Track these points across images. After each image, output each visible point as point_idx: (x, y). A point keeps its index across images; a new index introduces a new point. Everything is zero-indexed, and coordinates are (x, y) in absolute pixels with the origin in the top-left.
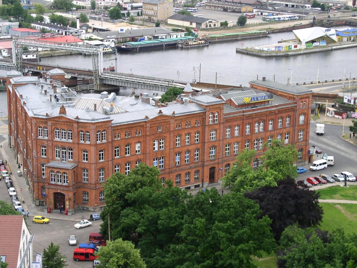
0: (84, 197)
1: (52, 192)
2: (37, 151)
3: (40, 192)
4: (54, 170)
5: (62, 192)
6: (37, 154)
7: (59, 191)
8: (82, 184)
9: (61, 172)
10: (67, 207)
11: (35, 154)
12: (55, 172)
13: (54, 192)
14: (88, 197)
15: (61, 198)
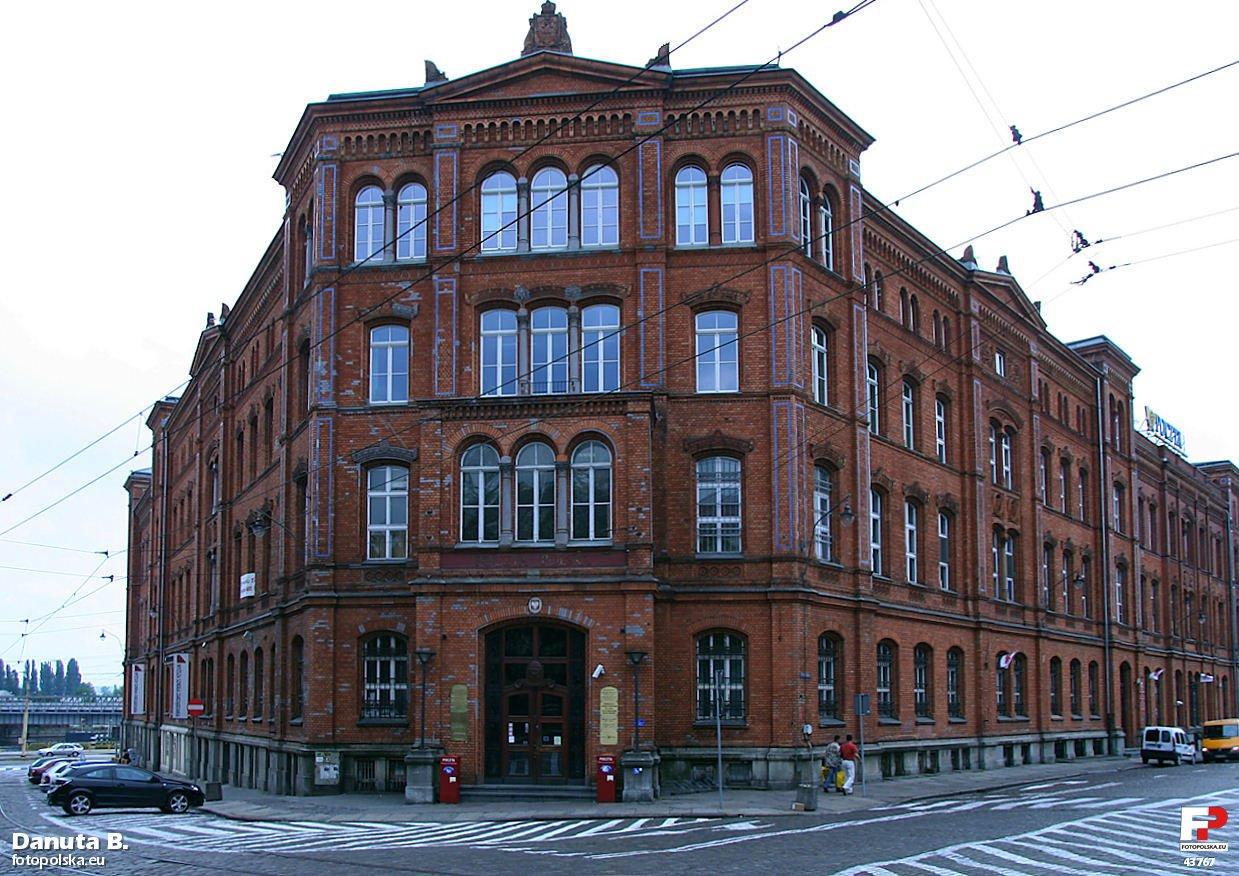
0: (706, 679)
1: (470, 621)
2: (338, 366)
3: (345, 687)
4: (493, 428)
5: (563, 614)
6: (338, 385)
7: (535, 605)
8: (694, 572)
9: (555, 435)
10: (608, 732)
11: (326, 387)
12: (506, 443)
13: (487, 619)
14: (734, 679)
15: (548, 670)
